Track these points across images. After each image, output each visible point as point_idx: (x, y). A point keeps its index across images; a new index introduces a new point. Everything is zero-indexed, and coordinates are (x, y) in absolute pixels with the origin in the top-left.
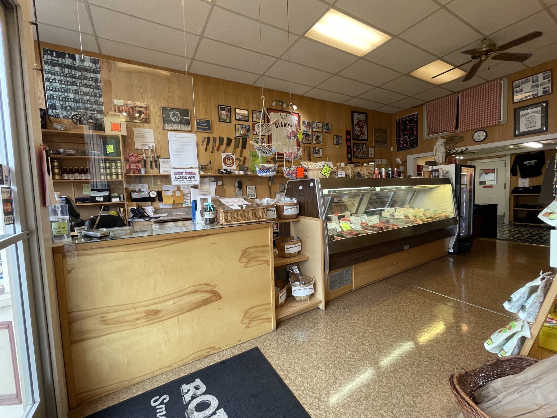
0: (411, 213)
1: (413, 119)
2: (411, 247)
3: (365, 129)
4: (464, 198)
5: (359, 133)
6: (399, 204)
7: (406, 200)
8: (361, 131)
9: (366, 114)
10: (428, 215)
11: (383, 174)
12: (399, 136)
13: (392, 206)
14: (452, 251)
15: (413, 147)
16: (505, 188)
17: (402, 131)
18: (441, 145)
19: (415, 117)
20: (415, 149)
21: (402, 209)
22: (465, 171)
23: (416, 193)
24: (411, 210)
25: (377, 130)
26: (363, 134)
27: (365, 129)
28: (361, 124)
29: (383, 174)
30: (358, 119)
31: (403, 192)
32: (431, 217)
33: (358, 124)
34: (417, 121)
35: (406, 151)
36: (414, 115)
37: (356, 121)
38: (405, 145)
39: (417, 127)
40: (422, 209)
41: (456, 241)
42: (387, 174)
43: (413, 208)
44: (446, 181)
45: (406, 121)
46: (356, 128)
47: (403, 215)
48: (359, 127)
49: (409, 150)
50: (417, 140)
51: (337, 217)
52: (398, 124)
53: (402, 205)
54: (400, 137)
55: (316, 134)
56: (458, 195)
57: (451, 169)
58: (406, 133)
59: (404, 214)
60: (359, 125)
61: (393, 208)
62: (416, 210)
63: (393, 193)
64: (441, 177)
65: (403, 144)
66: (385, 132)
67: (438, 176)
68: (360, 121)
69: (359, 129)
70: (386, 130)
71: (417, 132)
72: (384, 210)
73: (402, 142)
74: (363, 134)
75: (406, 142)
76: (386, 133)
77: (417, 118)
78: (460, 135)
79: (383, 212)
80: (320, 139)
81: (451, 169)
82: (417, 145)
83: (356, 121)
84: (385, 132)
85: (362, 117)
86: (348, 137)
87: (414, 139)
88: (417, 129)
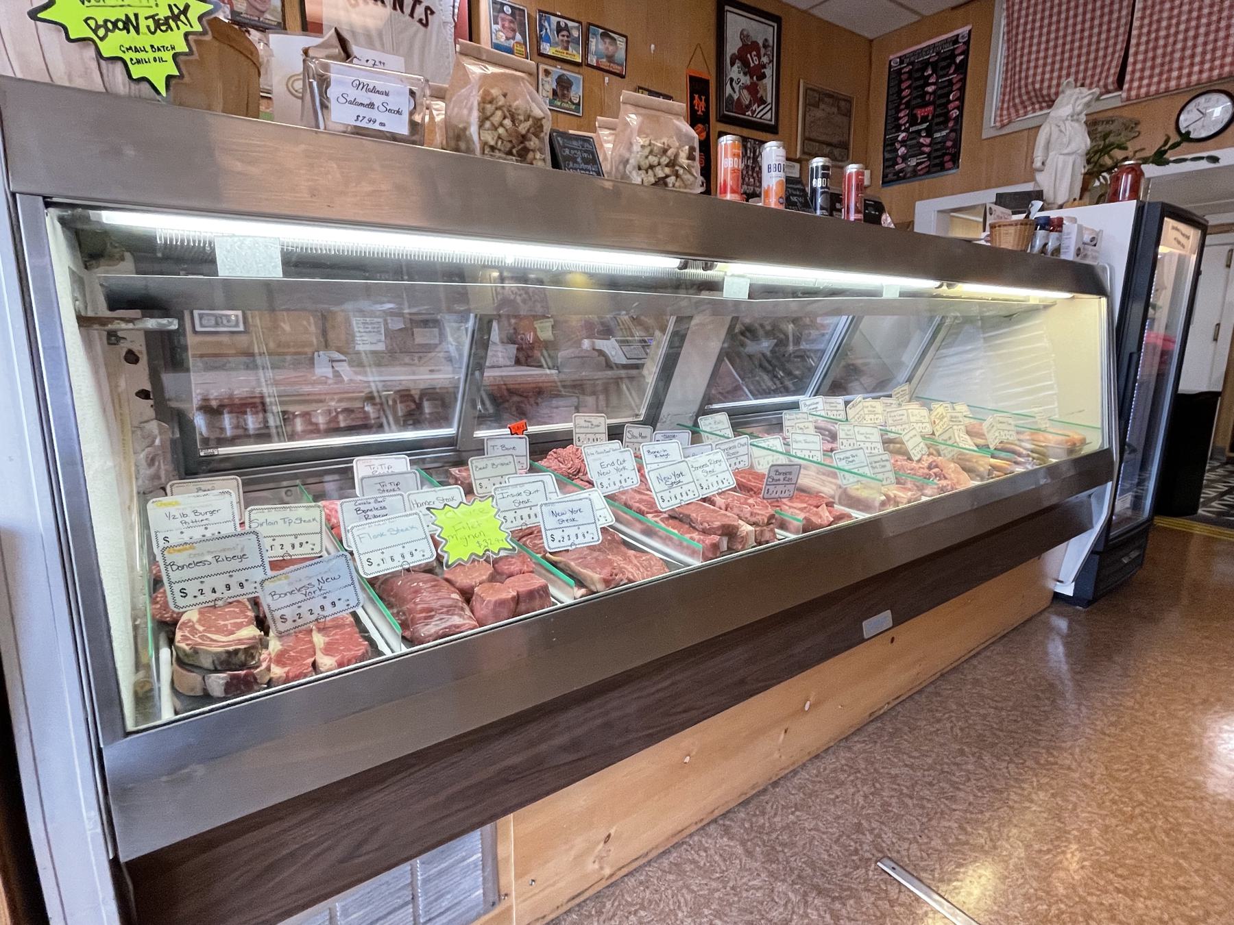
0: (911, 420)
1: (953, 55)
2: (897, 622)
3: (768, 83)
4: (1146, 369)
5: (746, 98)
6: (866, 380)
7: (900, 364)
8: (752, 89)
9: (777, 19)
10: (993, 441)
11: (772, 181)
12: (893, 125)
13: (836, 387)
14: (1068, 590)
15: (941, 167)
16: (1215, 339)
17: (908, 105)
18: (1074, 117)
19: (960, 47)
20: (951, 176)
21: (878, 405)
22: (1176, 243)
23: (946, 330)
24: (915, 411)
25: (816, 98)
26: (762, 101)
27: (768, 83)
28: (754, 61)
29: (772, 181)
30: (744, 36)
31: (887, 323)
32: (1005, 450)
33: (741, 57)
34: (964, 63)
35: (915, 185)
36: (955, 40)
37: (733, 46)
38: (913, 162)
39: (962, 90)
40: (962, 408)
41: (1093, 552)
42: (796, 192)
43: (926, 402)
44: (1085, 279)
45: (926, 64)
46: (734, 72)
47: (876, 437)
48: (747, 69)
49: (928, 182)
50: (957, 143)
51: (521, 446)
52: (895, 76)
53: (881, 386)
54: (898, 129)
55: (557, 70)
56: (1131, 345)
57: (1109, 226)
58: (920, 113)
59: (884, 432)
60: (745, 63)
61: (840, 400)
62: (939, 409)
63: (843, 320)
64: (1069, 255)
65: (905, 158)
66: (843, 105)
67: (1057, 250)
68: (749, 46)
69: (746, 80)
70: (849, 101)
71: (961, 108)
72: (795, 406)
73: (902, 151)
74: (762, 101)
75: (916, 150)
76: (848, 114)
77: (966, 53)
78: (1127, 113)
79: (787, 416)
80: (576, 93)
81: (1109, 226)
82: (955, 159)
83: (733, 46)
84: (843, 105)
85: (762, 32)
86: (700, 106)
87: (946, 138)
88: (961, 99)
